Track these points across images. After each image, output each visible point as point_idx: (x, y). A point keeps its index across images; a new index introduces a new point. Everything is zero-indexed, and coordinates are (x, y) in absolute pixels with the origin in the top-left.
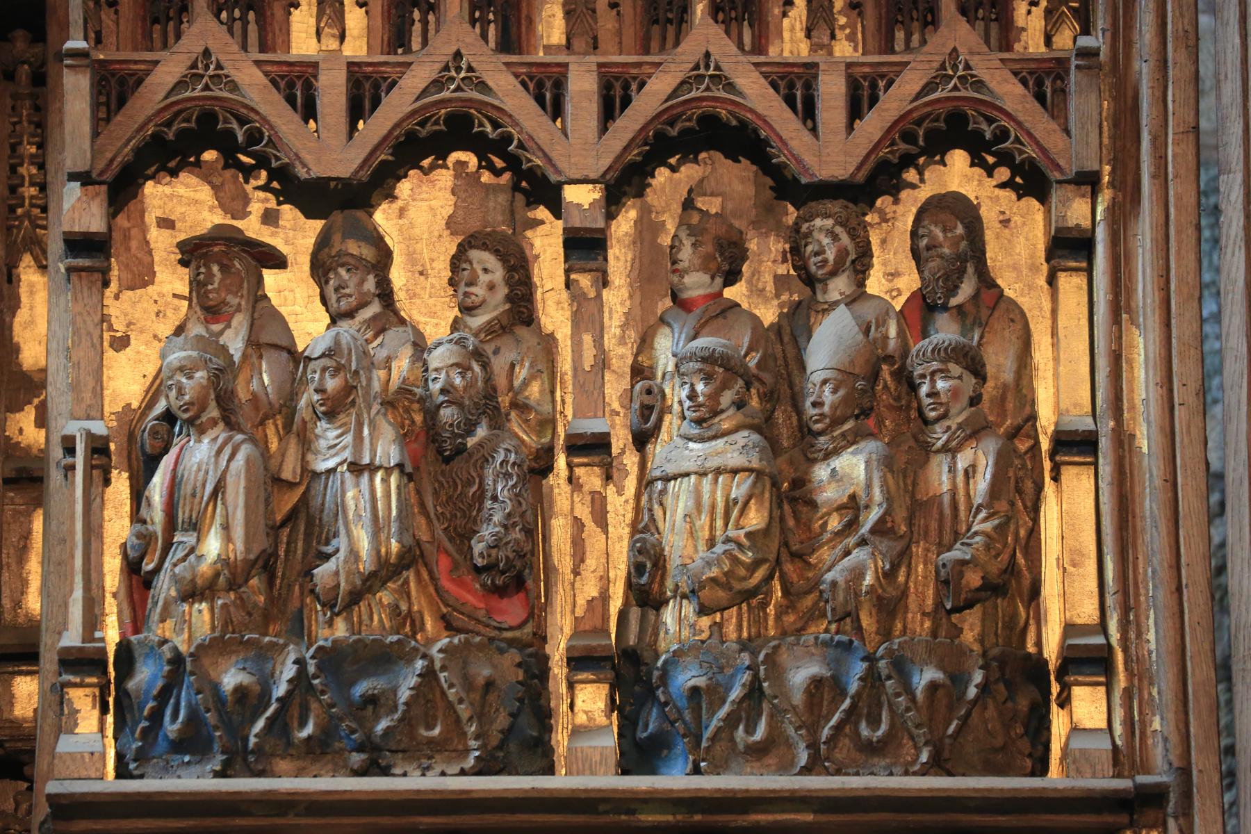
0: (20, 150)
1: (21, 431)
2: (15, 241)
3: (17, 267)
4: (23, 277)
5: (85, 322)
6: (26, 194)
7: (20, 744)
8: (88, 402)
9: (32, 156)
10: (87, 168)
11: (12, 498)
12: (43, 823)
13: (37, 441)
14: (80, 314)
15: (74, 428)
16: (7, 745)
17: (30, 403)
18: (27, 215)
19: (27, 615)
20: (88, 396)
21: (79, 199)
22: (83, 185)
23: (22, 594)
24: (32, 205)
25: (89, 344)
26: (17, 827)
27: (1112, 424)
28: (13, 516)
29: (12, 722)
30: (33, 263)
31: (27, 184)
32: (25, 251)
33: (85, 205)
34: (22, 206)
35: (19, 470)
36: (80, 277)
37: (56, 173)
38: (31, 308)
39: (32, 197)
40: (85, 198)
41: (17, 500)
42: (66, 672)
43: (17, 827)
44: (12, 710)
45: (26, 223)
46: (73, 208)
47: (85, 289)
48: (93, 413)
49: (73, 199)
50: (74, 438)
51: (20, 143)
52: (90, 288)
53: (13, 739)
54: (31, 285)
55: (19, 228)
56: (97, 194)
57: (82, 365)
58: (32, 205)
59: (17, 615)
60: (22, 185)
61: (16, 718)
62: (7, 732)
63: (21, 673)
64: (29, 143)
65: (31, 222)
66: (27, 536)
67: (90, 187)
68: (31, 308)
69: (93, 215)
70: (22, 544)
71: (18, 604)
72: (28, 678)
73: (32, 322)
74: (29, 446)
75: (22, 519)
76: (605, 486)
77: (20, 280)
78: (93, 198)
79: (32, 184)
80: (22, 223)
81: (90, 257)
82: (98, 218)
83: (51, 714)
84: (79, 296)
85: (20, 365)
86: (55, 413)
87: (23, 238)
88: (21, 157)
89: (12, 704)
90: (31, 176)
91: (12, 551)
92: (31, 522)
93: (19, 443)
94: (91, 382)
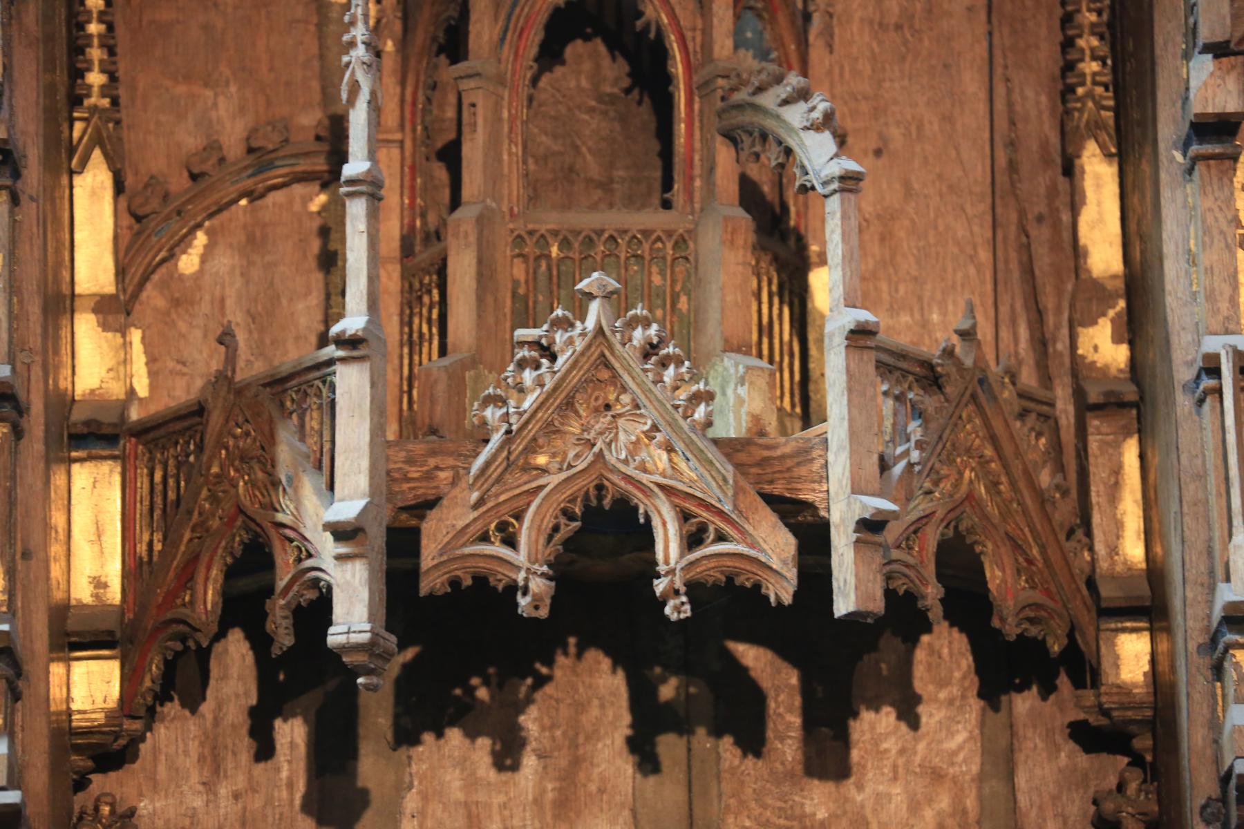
0: (1078, 18)
1: (1096, 348)
2: (1078, 127)
3: (1079, 157)
4: (1088, 168)
5: (1216, 219)
6: (1087, 71)
7: (1129, 713)
8: (1226, 313)
9: (1093, 25)
10: (1227, 37)
11: (1097, 428)
12: (1204, 808)
13: (1114, 360)
14: (1210, 210)
15: (1214, 344)
16: (1115, 714)
17: (1104, 314)
18: (1090, 95)
19: (1125, 562)
20: (1224, 306)
21: (1212, 74)
22: (1216, 57)
23: (1118, 537)
24: (1095, 83)
25: (1223, 245)
26: (1130, 810)
27: (1184, 46)
28: (1100, 448)
29: (1119, 687)
30: (1098, 151)
31: (1087, 58)
32: (1089, 138)
33: (1219, 81)
34: (1083, 84)
35: (1108, 394)
36: (1209, 166)
37: (1165, 44)
38: (1099, 204)
39: (1094, 74)
40: (1218, 73)
41: (1105, 429)
42: (1231, 631)
43: (1130, 810)
44: (1118, 674)
45: (1090, 104)
46: (1205, 84)
47: (1215, 180)
48: (1232, 327)
49: (1204, 76)
50: (1217, 357)
51: (1078, 11)
52: (1220, 179)
53: (1123, 707)
54: (1098, 177)
55: (1081, 110)
56: (1233, 67)
57: (1216, 271)
58: (1095, 83)
59: (1113, 563)
60: (1082, 60)
61: (1124, 683)
62: (1116, 699)
63: (1124, 630)
64: (1090, 10)
65: (1096, 103)
66: (1117, 471)
67: (1224, 60)
68: (1099, 204)
69: (1229, 92)
70: (1113, 480)
71: (1114, 550)
72: (1134, 636)
73: (1101, 220)
74: (1107, 366)
75: (1111, 451)
76: (15, 182)
77: (1083, 172)
78: (1228, 72)
79: (1094, 58)
80: (1084, 105)
81: (1220, 141)
82: (1235, 94)
83: (1201, 679)
84: (1209, 188)
85: (1089, 271)
86: (1177, 326)
87: (1088, 122)
88: (1080, 27)
89: (1118, 667)
90: (1092, 50)
91: (1102, 488)
92: (1121, 454)
93: (1094, 362)
94: (1227, 290)
